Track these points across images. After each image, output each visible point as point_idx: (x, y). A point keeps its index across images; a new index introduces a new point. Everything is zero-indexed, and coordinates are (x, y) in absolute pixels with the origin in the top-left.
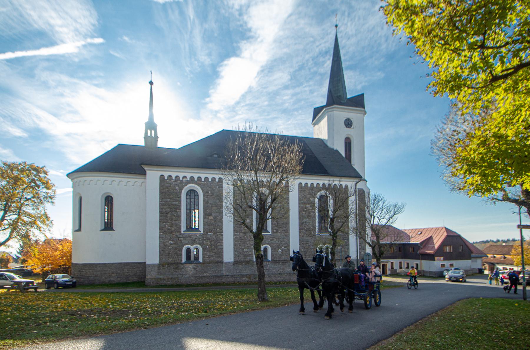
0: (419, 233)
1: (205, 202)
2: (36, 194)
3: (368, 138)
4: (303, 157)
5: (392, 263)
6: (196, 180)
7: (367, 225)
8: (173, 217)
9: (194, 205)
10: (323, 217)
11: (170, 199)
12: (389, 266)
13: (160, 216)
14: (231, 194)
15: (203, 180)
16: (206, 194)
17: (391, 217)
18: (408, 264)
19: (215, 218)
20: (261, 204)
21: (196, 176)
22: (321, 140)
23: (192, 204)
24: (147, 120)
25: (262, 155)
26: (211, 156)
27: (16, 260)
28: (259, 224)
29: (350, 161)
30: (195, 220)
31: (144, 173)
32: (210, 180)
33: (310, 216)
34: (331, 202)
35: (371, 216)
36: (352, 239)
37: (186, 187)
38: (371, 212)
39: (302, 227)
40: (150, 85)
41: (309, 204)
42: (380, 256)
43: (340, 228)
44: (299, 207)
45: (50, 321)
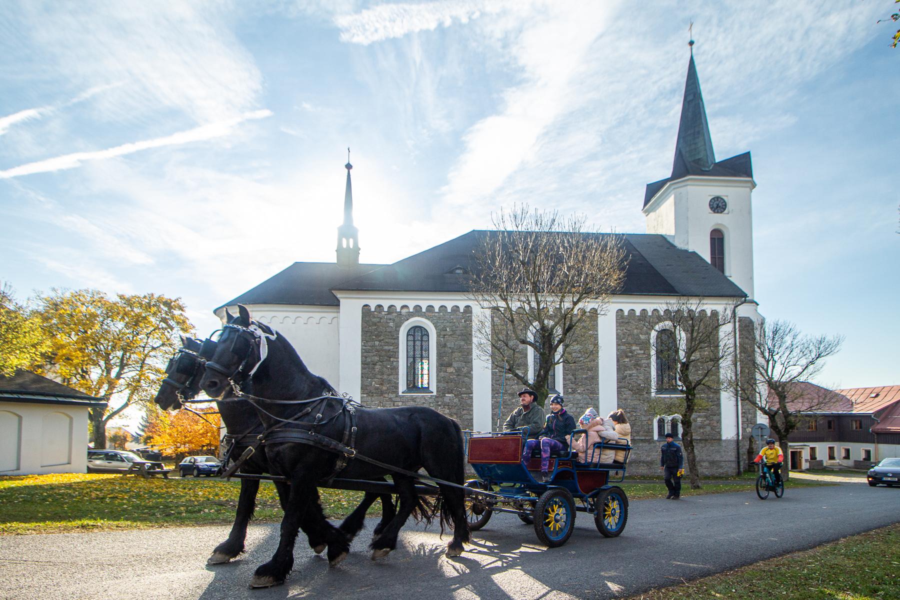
0: (873, 395)
1: (440, 346)
2: (168, 340)
3: (760, 234)
4: (626, 258)
5: (813, 449)
6: (424, 310)
7: (758, 376)
8: (385, 369)
9: (422, 350)
10: (665, 366)
11: (380, 341)
12: (806, 455)
13: (363, 368)
14: (488, 324)
15: (437, 310)
16: (443, 333)
17: (812, 363)
18: (848, 451)
19: (458, 370)
20: (544, 336)
21: (424, 305)
22: (662, 238)
23: (418, 348)
25: (546, 256)
26: (452, 272)
27: (136, 439)
28: (540, 370)
29: (722, 270)
30: (422, 374)
31: (336, 304)
32: (449, 310)
33: (640, 365)
34: (682, 337)
35: (768, 361)
36: (728, 403)
37: (406, 323)
38: (767, 354)
39: (622, 384)
41: (637, 345)
42: (787, 430)
43: (702, 380)
44: (617, 350)
45: (186, 512)
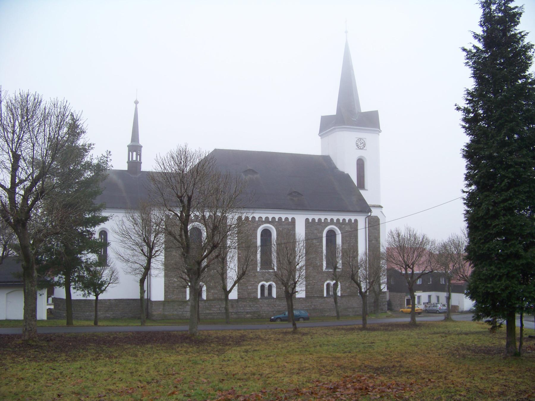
6: (270, 220)
21: (270, 217)
24: (129, 142)
40: (135, 105)
